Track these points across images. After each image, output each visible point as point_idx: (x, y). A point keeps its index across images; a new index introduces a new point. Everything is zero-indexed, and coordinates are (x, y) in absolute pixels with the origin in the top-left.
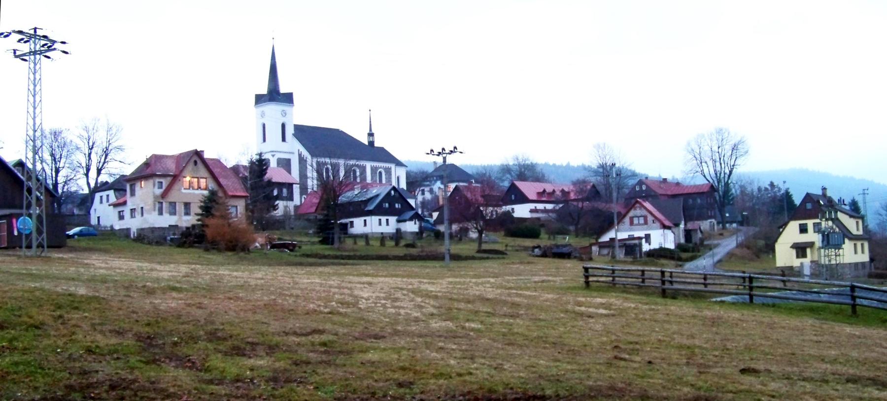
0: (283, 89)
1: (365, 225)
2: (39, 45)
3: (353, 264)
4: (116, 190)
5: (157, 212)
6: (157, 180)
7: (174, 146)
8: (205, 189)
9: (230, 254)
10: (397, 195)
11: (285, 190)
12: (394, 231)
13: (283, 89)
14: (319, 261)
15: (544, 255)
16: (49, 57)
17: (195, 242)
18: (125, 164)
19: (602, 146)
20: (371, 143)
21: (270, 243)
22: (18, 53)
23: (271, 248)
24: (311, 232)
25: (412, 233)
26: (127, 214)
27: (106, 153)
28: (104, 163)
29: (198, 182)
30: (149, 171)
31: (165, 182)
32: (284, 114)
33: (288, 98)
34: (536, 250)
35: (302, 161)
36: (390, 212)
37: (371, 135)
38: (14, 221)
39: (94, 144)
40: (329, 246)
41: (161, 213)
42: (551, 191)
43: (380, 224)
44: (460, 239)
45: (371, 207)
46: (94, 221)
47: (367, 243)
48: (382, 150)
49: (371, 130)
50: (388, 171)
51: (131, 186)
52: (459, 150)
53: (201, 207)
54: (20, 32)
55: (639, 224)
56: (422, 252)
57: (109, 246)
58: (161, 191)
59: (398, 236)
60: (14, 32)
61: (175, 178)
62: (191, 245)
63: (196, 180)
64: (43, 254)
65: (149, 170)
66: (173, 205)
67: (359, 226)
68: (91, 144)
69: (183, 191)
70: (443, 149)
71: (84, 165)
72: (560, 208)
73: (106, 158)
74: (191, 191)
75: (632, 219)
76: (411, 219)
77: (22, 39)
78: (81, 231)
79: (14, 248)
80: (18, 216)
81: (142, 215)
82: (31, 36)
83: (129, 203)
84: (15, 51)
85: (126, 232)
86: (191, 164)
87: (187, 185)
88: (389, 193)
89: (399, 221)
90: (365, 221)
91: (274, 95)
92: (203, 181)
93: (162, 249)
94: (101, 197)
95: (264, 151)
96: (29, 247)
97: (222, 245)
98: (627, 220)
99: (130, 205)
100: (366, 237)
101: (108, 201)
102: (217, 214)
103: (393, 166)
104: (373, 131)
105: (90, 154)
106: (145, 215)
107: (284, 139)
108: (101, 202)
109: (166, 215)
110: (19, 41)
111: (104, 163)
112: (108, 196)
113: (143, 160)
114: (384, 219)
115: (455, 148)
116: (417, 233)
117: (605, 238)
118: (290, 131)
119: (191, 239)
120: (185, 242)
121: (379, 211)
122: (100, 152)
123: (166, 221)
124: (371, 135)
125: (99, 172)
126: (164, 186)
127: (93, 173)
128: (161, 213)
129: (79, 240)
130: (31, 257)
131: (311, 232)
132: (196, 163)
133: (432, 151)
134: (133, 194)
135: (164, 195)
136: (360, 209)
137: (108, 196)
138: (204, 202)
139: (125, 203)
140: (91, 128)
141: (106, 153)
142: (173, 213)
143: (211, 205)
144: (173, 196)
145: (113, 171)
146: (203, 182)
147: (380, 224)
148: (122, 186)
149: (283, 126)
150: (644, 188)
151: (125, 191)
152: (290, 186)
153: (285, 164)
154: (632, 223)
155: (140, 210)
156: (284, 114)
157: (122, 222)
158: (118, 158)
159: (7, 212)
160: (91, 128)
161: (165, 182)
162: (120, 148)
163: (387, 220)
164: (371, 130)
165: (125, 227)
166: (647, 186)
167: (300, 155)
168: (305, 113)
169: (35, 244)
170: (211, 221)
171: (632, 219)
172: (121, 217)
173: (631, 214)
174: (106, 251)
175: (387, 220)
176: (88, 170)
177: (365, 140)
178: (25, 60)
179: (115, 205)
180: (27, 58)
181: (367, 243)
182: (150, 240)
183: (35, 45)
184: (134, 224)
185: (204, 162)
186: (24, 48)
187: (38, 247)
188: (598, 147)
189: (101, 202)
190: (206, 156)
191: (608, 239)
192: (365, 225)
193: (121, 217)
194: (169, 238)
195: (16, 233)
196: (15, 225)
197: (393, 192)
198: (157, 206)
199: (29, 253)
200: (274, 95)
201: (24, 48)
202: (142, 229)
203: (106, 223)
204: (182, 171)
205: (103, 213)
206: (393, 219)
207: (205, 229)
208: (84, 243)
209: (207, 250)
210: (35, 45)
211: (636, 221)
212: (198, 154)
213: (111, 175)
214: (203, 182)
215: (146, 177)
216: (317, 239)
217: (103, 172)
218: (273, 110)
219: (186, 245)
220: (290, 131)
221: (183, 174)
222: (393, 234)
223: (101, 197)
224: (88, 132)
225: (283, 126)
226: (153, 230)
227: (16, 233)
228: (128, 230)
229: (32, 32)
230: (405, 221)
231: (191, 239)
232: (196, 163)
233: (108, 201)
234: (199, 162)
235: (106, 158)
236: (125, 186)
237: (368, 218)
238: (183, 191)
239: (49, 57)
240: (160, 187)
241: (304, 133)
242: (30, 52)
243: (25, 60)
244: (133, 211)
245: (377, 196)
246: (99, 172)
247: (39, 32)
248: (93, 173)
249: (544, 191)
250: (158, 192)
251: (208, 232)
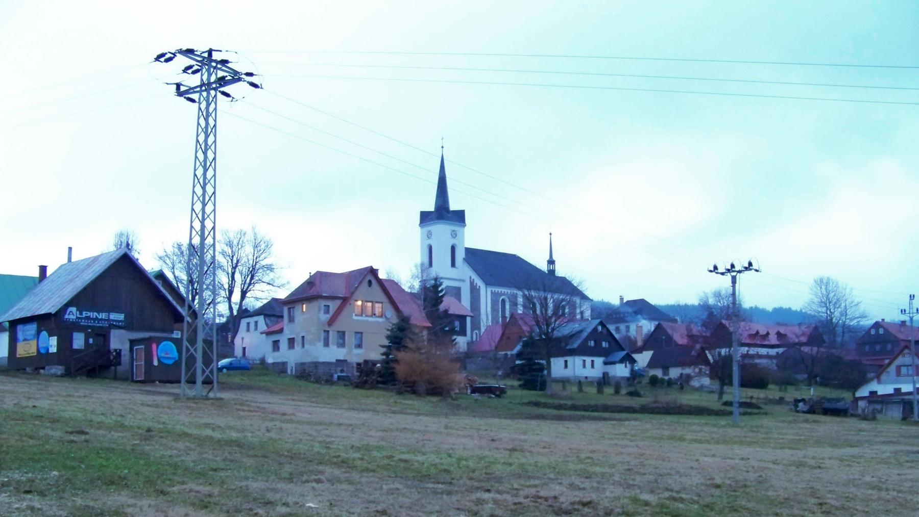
0: (454, 206)
1: (566, 366)
2: (212, 76)
3: (620, 420)
4: (266, 316)
5: (322, 343)
6: (323, 303)
7: (342, 262)
8: (381, 316)
9: (434, 399)
10: (605, 331)
11: (457, 324)
12: (601, 375)
13: (454, 206)
14: (555, 412)
15: (811, 411)
16: (227, 95)
17: (378, 382)
18: (285, 280)
19: (825, 281)
20: (552, 272)
21: (471, 386)
22: (183, 89)
23: (473, 391)
24: (500, 373)
25: (623, 378)
26: (284, 345)
27: (252, 272)
28: (250, 284)
29: (373, 307)
30: (313, 292)
31: (334, 305)
32: (454, 235)
33: (459, 217)
34: (801, 404)
35: (474, 290)
36: (596, 352)
37: (551, 262)
38: (154, 346)
39: (238, 261)
40: (541, 393)
41: (326, 344)
42: (765, 333)
43: (584, 366)
44: (682, 388)
45: (576, 344)
46: (238, 352)
47: (580, 390)
48: (563, 280)
49: (551, 256)
50: (573, 306)
51: (289, 309)
52: (755, 266)
53: (388, 337)
54: (189, 52)
55: (908, 375)
56: (655, 402)
57: (269, 384)
58: (328, 316)
59: (604, 381)
60: (181, 52)
61: (345, 300)
62: (374, 386)
63: (369, 304)
64: (211, 395)
65: (314, 290)
66: (342, 334)
67: (558, 367)
68: (235, 261)
69: (355, 318)
70: (733, 266)
71: (226, 286)
72: (783, 353)
73: (252, 278)
74: (364, 318)
75: (898, 368)
76: (621, 361)
77: (190, 67)
78: (231, 363)
79: (153, 382)
80: (159, 341)
81: (303, 346)
82: (208, 60)
83: (286, 330)
84: (178, 86)
85: (281, 368)
86: (365, 284)
87: (358, 310)
88: (595, 329)
89: (605, 363)
90: (566, 361)
91: (443, 213)
92: (378, 306)
93: (326, 390)
94: (248, 324)
95: (441, 276)
96: (192, 381)
97: (422, 387)
98: (892, 368)
99: (288, 333)
100: (564, 382)
101: (256, 329)
102: (410, 345)
103: (578, 300)
104: (554, 258)
105: (233, 274)
106: (306, 346)
107: (453, 264)
108: (248, 330)
109: (333, 347)
110: (185, 70)
111: (250, 284)
112: (256, 322)
113: (306, 277)
114: (588, 360)
115: (750, 264)
116: (628, 379)
117: (864, 392)
118: (460, 255)
119: (375, 378)
120: (366, 382)
121: (583, 351)
122: (245, 270)
123: (331, 354)
124: (551, 262)
125: (244, 294)
126: (332, 310)
127: (236, 297)
128: (326, 344)
129: (229, 375)
130: (193, 399)
131: (500, 373)
132: (370, 283)
133: (716, 268)
134: (291, 320)
135: (331, 322)
136: (562, 347)
137: (256, 322)
138: (392, 331)
139: (281, 331)
140: (235, 242)
141: (252, 272)
142: (342, 345)
143: (399, 337)
144: (339, 325)
145: (259, 294)
146: (378, 308)
147: (584, 366)
148: (273, 311)
149: (453, 249)
150: (881, 331)
151: (282, 317)
152: (462, 318)
153: (457, 292)
154: (898, 373)
155: (300, 340)
156: (454, 235)
157: (276, 354)
158: (266, 279)
159: (146, 335)
160: (235, 242)
161: (334, 305)
162: (270, 268)
163: (593, 361)
164: (551, 256)
165: (279, 360)
166: (885, 330)
167: (472, 283)
168: (476, 236)
169: (200, 379)
170: (402, 355)
171: (898, 368)
172: (276, 345)
173: (898, 362)
174: (268, 390)
175: (593, 361)
176: (231, 292)
177: (543, 266)
178: (193, 101)
179: (268, 334)
180: (195, 96)
181: (580, 390)
182: (312, 375)
183: (210, 75)
184: (291, 357)
185: (380, 281)
186: (193, 80)
187: (204, 383)
188: (823, 283)
189: (248, 330)
190: (382, 275)
191: (867, 394)
192: (566, 366)
193: (276, 345)
194: (336, 376)
195: (156, 363)
196: (155, 353)
197: (600, 328)
198: (323, 335)
199: (191, 393)
200: (443, 213)
201: (193, 80)
202: (303, 364)
203: (254, 354)
204: (353, 293)
205: (251, 341)
206: (599, 361)
207: (392, 365)
208: (236, 379)
209: (400, 393)
210: (210, 75)
211: (904, 370)
212: (373, 272)
213: (257, 299)
214: (378, 308)
215: (309, 299)
216: (516, 383)
217: (248, 295)
218: (441, 230)
219: (367, 386)
220: (460, 255)
221: (355, 297)
222: (600, 379)
223: (248, 324)
224: (231, 247)
225: (453, 249)
226: (316, 365)
227: (156, 363)
228: (284, 364)
229: (206, 55)
230: (613, 363)
231: (375, 378)
232: (370, 283)
233: (256, 329)
234: (374, 282)
235: (252, 278)
236: (282, 312)
237: (570, 359)
238: (355, 318)
239: (227, 95)
240: (327, 311)
241: (476, 258)
242: (201, 86)
243: (193, 101)
244: (291, 341)
245: (581, 332)
246: (244, 294)
247: (216, 56)
248: (236, 297)
249: (758, 332)
250: (325, 317)
251: (400, 370)
